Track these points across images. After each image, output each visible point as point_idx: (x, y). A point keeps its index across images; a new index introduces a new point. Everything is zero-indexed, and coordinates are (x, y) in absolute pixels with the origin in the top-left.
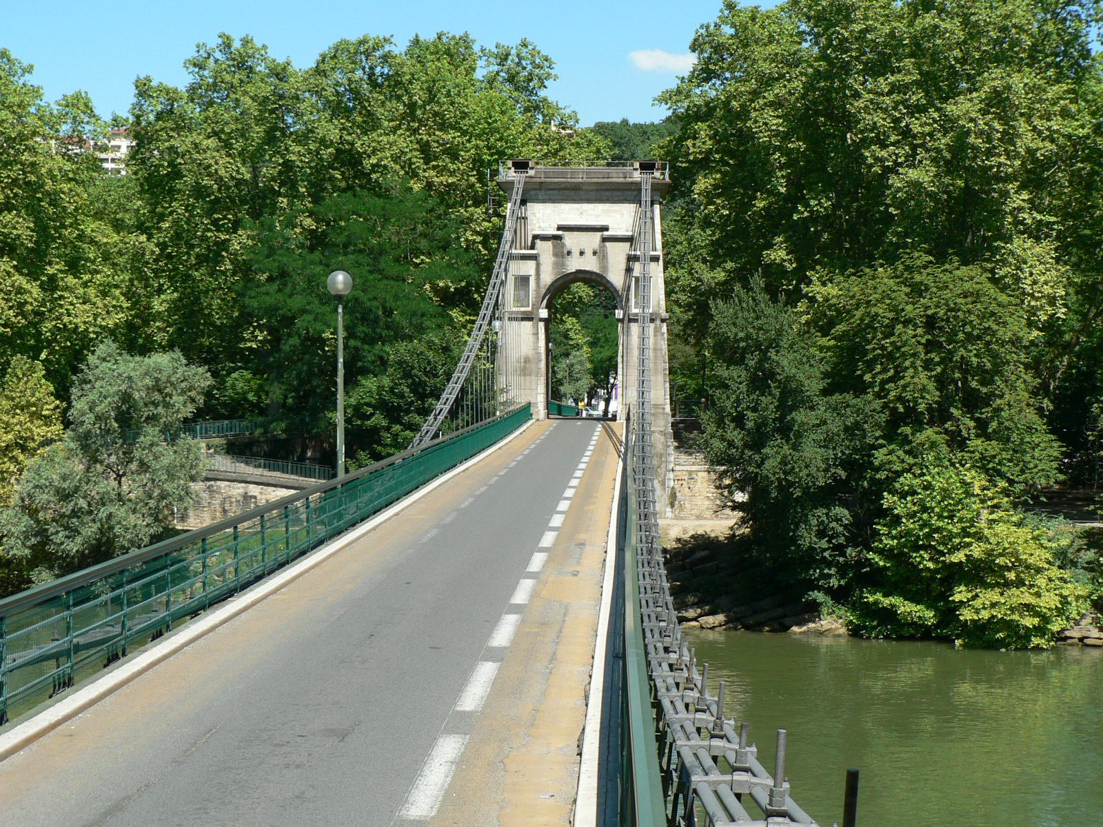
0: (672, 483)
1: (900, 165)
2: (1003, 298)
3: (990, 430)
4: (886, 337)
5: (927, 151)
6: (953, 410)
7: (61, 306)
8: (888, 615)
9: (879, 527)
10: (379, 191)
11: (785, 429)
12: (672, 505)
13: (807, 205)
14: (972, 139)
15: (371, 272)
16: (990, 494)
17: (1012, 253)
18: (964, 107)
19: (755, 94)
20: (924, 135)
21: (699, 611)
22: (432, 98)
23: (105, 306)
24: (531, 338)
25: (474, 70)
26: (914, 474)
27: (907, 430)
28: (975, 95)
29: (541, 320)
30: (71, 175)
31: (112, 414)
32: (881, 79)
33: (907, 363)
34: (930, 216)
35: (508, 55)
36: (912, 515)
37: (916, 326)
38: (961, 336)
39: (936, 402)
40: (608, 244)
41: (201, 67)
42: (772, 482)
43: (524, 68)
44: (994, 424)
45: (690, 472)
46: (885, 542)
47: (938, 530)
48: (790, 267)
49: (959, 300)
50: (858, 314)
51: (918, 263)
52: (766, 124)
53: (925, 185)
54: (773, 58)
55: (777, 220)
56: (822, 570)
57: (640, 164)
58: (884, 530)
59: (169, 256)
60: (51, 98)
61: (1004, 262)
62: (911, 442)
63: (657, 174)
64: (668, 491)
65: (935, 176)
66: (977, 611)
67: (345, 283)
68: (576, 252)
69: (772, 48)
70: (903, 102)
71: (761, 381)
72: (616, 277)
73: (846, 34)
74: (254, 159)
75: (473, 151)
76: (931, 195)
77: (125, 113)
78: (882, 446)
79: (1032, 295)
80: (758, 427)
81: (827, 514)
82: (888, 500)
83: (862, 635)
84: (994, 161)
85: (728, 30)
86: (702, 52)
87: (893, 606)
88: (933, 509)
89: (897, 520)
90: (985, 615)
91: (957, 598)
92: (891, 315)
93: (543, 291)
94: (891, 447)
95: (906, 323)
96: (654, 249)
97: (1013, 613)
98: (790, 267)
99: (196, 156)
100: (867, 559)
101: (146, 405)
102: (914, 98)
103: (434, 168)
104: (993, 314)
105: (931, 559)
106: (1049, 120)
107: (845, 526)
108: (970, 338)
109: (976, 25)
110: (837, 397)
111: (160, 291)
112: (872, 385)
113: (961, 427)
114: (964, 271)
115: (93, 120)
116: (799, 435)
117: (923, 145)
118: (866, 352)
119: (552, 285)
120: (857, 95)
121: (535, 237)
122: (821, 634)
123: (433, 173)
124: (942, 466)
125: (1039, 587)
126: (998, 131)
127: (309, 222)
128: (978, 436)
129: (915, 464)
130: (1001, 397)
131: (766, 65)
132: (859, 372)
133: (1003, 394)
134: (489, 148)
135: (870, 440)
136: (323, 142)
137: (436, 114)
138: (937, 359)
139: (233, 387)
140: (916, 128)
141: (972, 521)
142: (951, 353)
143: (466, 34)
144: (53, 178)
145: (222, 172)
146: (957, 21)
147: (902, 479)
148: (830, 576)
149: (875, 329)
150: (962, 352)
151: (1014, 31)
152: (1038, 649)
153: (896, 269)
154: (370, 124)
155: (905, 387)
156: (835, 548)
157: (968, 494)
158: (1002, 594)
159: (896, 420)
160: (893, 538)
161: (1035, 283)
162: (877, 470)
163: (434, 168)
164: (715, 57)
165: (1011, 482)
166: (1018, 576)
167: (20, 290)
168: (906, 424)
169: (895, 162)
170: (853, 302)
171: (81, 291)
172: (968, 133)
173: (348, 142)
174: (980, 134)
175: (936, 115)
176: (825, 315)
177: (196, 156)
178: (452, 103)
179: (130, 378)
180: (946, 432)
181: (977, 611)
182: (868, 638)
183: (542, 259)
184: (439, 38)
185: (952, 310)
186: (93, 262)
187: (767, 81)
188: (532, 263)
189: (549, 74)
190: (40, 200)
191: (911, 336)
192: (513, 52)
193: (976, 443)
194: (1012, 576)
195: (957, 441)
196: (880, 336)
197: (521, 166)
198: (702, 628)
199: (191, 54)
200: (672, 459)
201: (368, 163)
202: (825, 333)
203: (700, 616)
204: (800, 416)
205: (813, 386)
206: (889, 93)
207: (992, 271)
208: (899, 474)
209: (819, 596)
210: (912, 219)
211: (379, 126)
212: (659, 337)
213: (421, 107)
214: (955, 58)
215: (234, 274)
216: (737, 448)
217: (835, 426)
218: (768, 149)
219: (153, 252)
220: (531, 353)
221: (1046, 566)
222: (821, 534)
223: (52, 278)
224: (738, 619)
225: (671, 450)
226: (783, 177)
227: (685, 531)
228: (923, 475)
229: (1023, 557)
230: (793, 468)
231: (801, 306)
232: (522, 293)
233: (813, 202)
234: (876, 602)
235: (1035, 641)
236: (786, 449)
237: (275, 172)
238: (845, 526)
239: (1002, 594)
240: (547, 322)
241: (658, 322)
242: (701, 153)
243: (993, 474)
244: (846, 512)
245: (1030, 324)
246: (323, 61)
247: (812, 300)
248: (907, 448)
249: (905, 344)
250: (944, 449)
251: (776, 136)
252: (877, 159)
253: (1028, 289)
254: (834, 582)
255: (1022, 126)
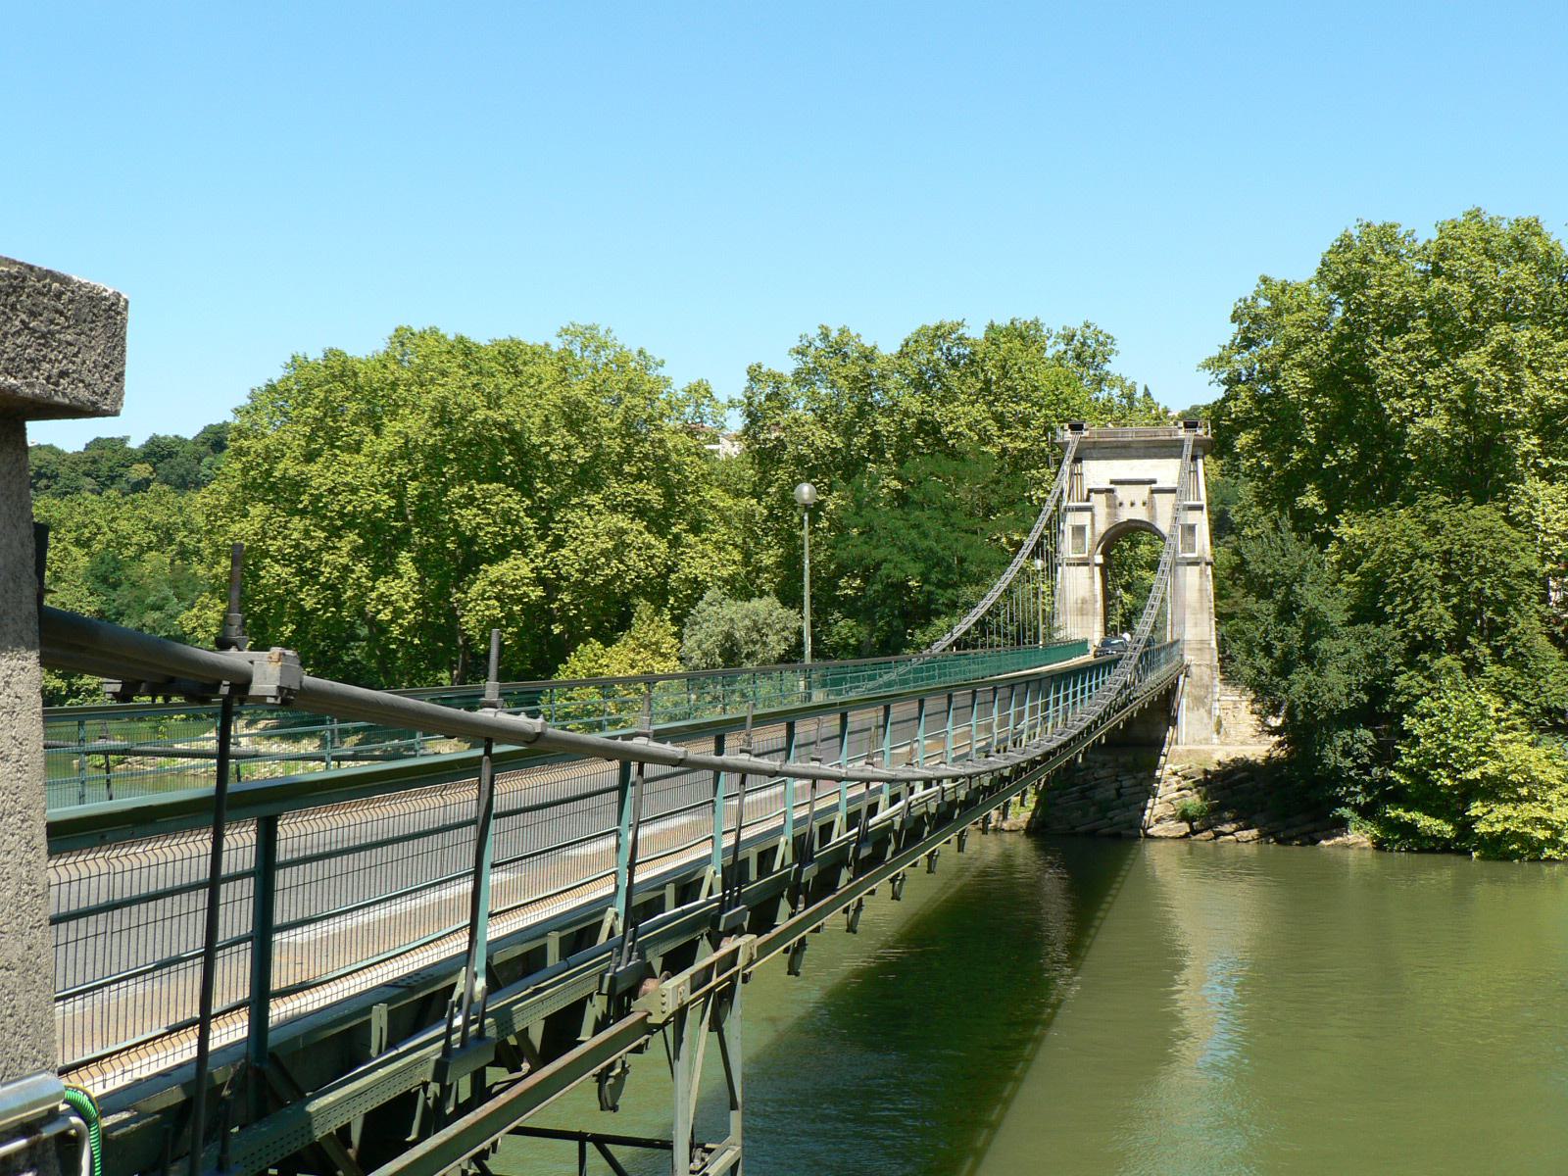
0: (1217, 713)
1: (1417, 415)
2: (1515, 534)
3: (1505, 657)
4: (1405, 570)
5: (1441, 401)
6: (1469, 638)
7: (683, 560)
8: (1409, 829)
9: (1399, 747)
10: (953, 454)
11: (1309, 657)
12: (1218, 733)
13: (1335, 455)
14: (1479, 389)
15: (944, 525)
16: (1503, 715)
17: (1525, 493)
18: (1473, 361)
19: (1285, 356)
20: (1438, 388)
21: (1234, 826)
22: (1006, 375)
23: (720, 559)
24: (1088, 581)
25: (1045, 349)
26: (1432, 697)
27: (1426, 657)
28: (1482, 349)
29: (1097, 565)
30: (693, 450)
31: (717, 651)
32: (1396, 339)
33: (1425, 595)
34: (1446, 460)
35: (1074, 336)
36: (1430, 736)
37: (1433, 560)
38: (1475, 570)
39: (1453, 631)
40: (1155, 495)
41: (803, 354)
42: (1298, 706)
43: (1089, 347)
44: (1509, 651)
45: (1235, 702)
46: (1405, 761)
47: (1455, 749)
48: (1321, 511)
49: (1473, 536)
50: (1378, 550)
51: (1434, 503)
52: (1294, 382)
53: (1439, 432)
54: (1301, 324)
55: (1309, 471)
56: (1348, 788)
57: (1185, 424)
58: (1404, 750)
59: (777, 518)
60: (679, 386)
61: (1518, 501)
62: (1429, 668)
63: (1200, 432)
64: (1215, 719)
65: (1449, 424)
66: (1491, 824)
67: (810, 494)
68: (1127, 504)
69: (1303, 315)
70: (1417, 358)
71: (1287, 612)
72: (1163, 525)
73: (1363, 299)
74: (848, 431)
75: (1042, 420)
76: (1446, 441)
77: (738, 395)
78: (1403, 672)
79: (1545, 532)
80: (1285, 654)
81: (1352, 737)
82: (1408, 722)
83: (1386, 848)
84: (1502, 408)
85: (1264, 303)
86: (1241, 323)
87: (1413, 820)
88: (1448, 729)
89: (1416, 740)
90: (1499, 828)
91: (1473, 813)
92: (1409, 551)
93: (1098, 539)
94: (1411, 673)
95: (1423, 558)
96: (1199, 499)
97: (1525, 825)
98: (1321, 511)
99: (795, 429)
100: (1391, 778)
101: (746, 643)
102: (1428, 354)
103: (1008, 435)
104: (1506, 548)
105: (1449, 777)
106: (1557, 371)
107: (1370, 747)
108: (1484, 571)
109: (1482, 287)
110: (1360, 627)
111: (769, 546)
112: (1393, 615)
113: (1477, 654)
114: (1478, 510)
115: (713, 403)
116: (1323, 663)
117: (1437, 397)
118: (1386, 586)
119: (1106, 532)
120: (1375, 354)
121: (1090, 491)
122: (1348, 847)
123: (1007, 440)
124: (1459, 691)
125: (1551, 802)
126: (1504, 381)
127: (895, 484)
128: (1494, 662)
129: (1434, 689)
130: (1515, 626)
131: (1293, 330)
132: (1380, 605)
133: (1517, 623)
134: (1057, 417)
135: (1390, 667)
136: (906, 414)
137: (1009, 389)
138: (1453, 591)
139: (839, 633)
140: (1430, 381)
141: (1488, 739)
142: (1466, 585)
143: (1037, 320)
144: (677, 452)
145: (818, 442)
146: (1465, 285)
147: (1421, 702)
148: (1357, 794)
149: (1395, 564)
150: (1477, 584)
151: (1517, 292)
152: (1550, 859)
153: (1415, 510)
154: (948, 397)
155: (1422, 617)
156: (1359, 767)
157: (1483, 716)
158: (1515, 809)
159: (1415, 649)
160: (1413, 757)
161: (1547, 520)
162: (1398, 694)
163: (1008, 435)
164: (1254, 327)
165: (1528, 705)
166: (1530, 792)
167: (649, 547)
168: (1426, 653)
169: (1412, 412)
170: (1373, 539)
171: (700, 547)
172: (1476, 382)
173: (929, 413)
174: (1488, 384)
175: (1449, 369)
176: (1353, 554)
177: (795, 429)
178: (1023, 379)
179: (732, 620)
180: (1464, 659)
181: (1491, 824)
182: (1391, 851)
183: (1096, 510)
184: (1012, 323)
185: (1466, 546)
186: (712, 522)
187: (1295, 344)
188: (1088, 514)
189: (1112, 350)
190: (667, 469)
191: (1431, 570)
192: (1079, 333)
193: (1492, 669)
194: (1524, 791)
195: (1473, 668)
196: (1399, 570)
197: (1077, 428)
198: (1238, 841)
199: (796, 344)
200: (1218, 689)
201: (944, 431)
202: (1352, 572)
203: (1236, 830)
204: (1323, 644)
205: (1337, 616)
206: (1404, 351)
207: (1506, 510)
208: (1418, 697)
209: (1346, 812)
210: (1431, 467)
211: (956, 399)
212: (1204, 579)
213: (995, 383)
214: (1465, 318)
215: (830, 531)
216: (1266, 675)
217: (1357, 654)
218: (1296, 406)
219: (761, 514)
220: (1087, 595)
221: (1558, 782)
222: (1346, 753)
223: (677, 537)
224: (1272, 834)
225: (1217, 682)
226: (1312, 429)
227: (1228, 755)
228: (1440, 698)
229: (1534, 774)
230: (1317, 693)
231: (1332, 547)
232: (1079, 541)
233: (1340, 452)
234: (1398, 817)
235: (1548, 852)
236: (1311, 676)
237: (864, 441)
238: (1370, 747)
239: (1515, 809)
240: (1104, 568)
241: (1203, 565)
242: (1241, 411)
243: (1508, 698)
244: (1370, 734)
245: (1543, 559)
246: (907, 344)
247: (1340, 540)
248: (1426, 674)
249: (1423, 577)
250: (1461, 675)
251: (1303, 393)
252: (1395, 410)
253: (1542, 527)
254: (1360, 799)
255: (1527, 375)
